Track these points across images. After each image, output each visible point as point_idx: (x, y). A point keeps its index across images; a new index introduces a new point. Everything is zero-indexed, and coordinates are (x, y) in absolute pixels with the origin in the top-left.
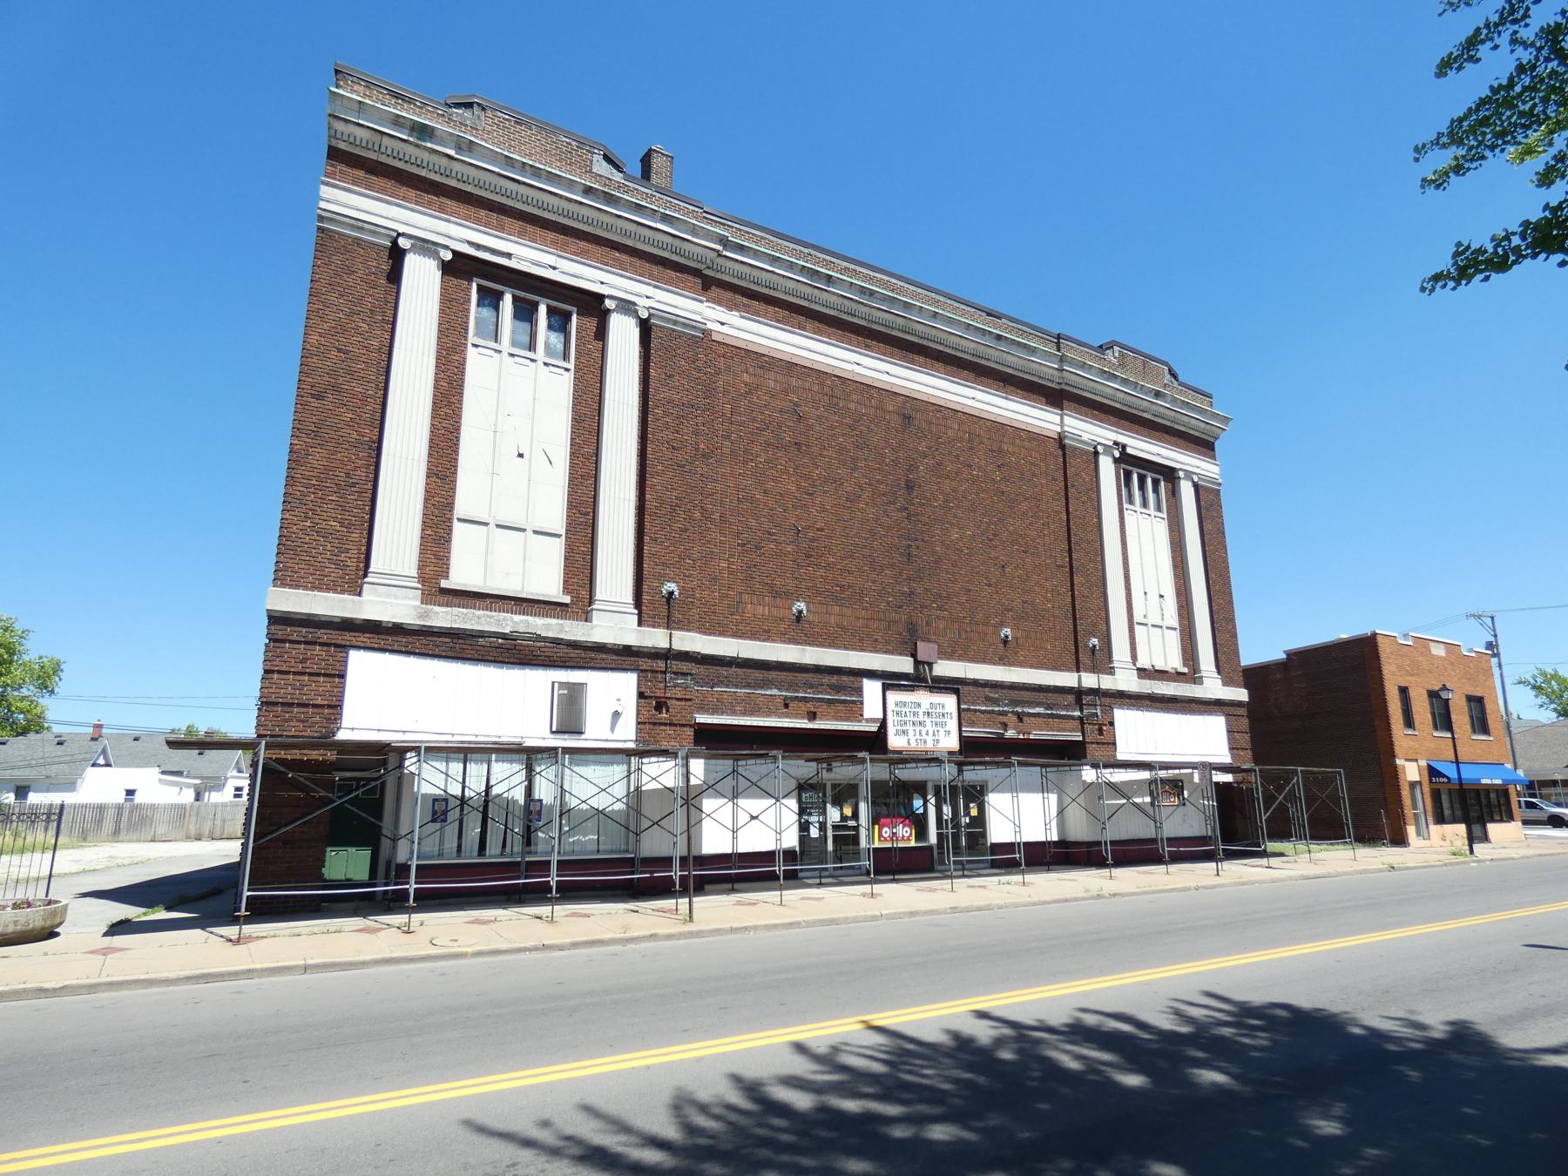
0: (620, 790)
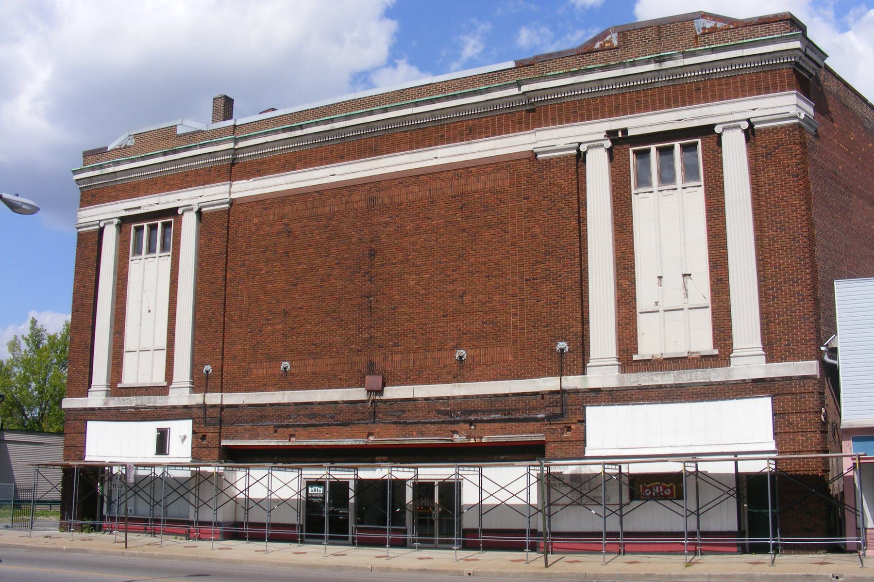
0: (295, 485)
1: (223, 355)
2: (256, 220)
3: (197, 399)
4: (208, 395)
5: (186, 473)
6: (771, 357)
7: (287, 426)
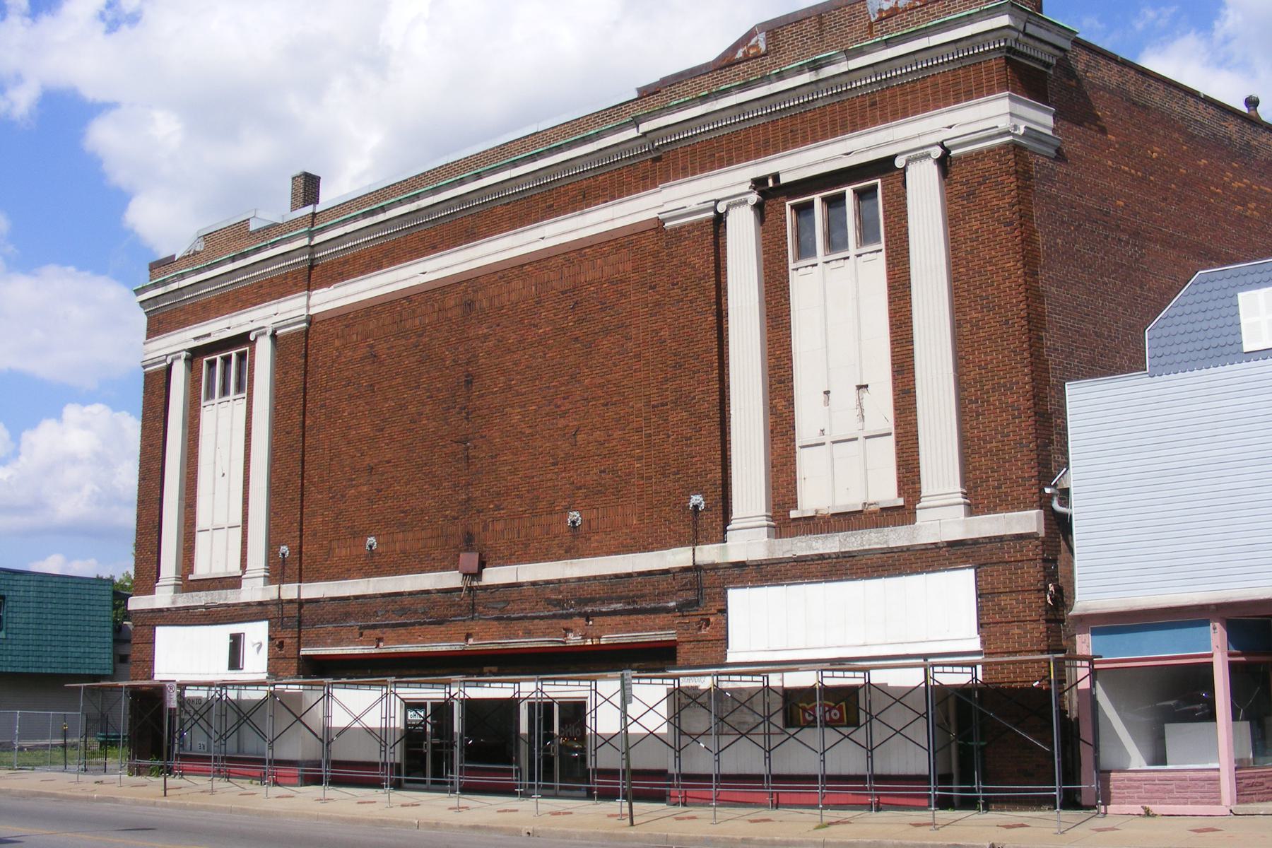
1: (301, 530)
2: (337, 343)
3: (271, 593)
4: (284, 586)
5: (258, 694)
6: (973, 509)
7: (374, 627)
